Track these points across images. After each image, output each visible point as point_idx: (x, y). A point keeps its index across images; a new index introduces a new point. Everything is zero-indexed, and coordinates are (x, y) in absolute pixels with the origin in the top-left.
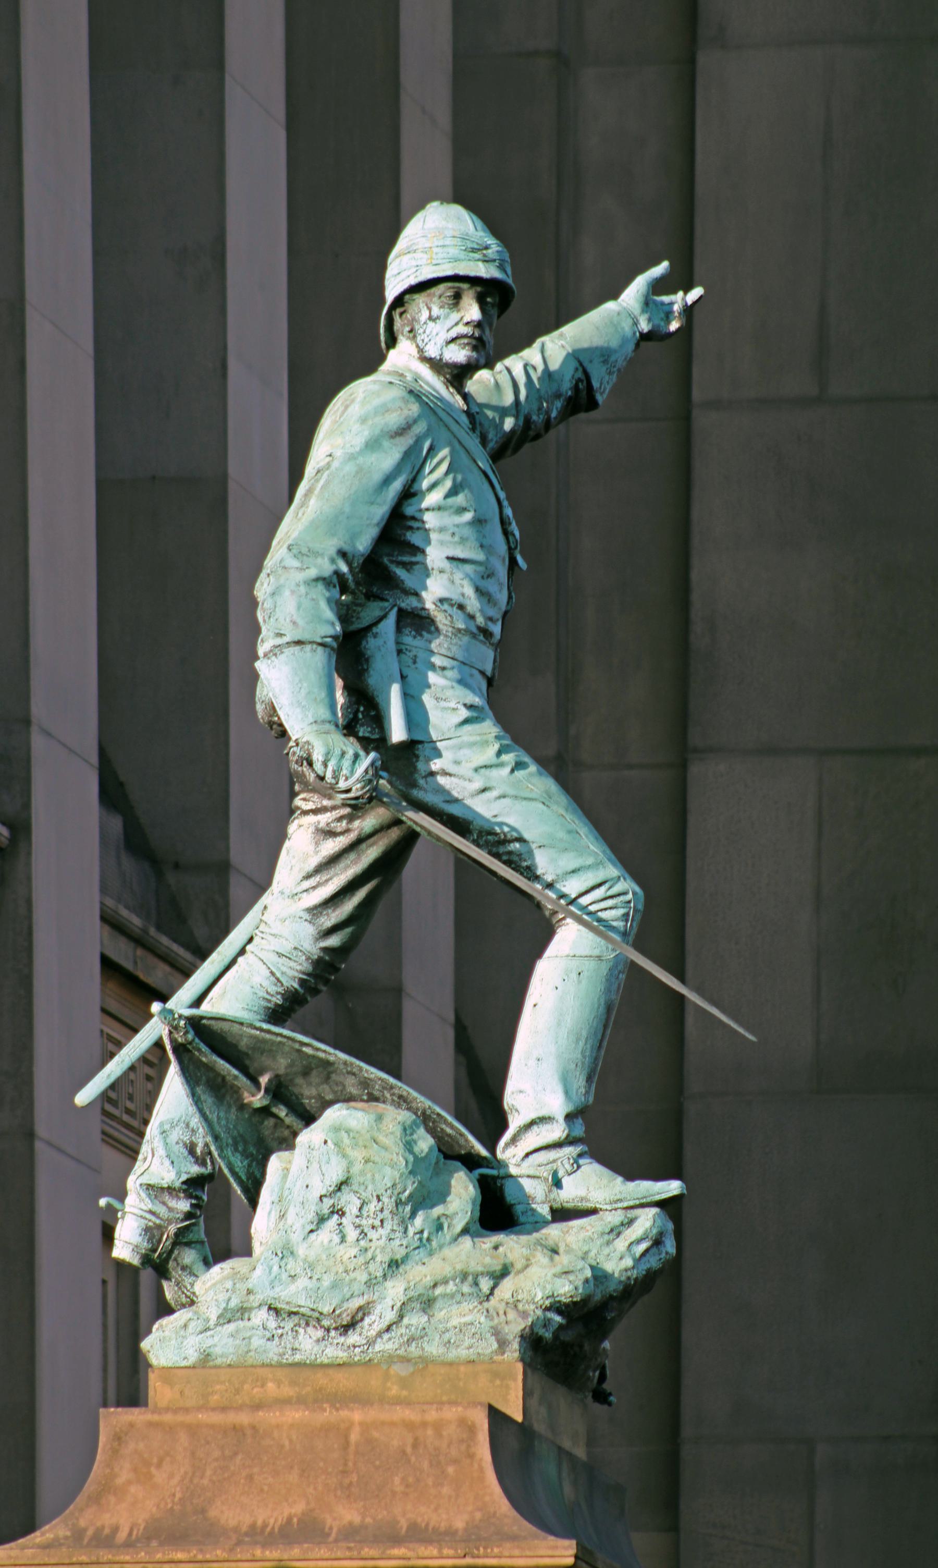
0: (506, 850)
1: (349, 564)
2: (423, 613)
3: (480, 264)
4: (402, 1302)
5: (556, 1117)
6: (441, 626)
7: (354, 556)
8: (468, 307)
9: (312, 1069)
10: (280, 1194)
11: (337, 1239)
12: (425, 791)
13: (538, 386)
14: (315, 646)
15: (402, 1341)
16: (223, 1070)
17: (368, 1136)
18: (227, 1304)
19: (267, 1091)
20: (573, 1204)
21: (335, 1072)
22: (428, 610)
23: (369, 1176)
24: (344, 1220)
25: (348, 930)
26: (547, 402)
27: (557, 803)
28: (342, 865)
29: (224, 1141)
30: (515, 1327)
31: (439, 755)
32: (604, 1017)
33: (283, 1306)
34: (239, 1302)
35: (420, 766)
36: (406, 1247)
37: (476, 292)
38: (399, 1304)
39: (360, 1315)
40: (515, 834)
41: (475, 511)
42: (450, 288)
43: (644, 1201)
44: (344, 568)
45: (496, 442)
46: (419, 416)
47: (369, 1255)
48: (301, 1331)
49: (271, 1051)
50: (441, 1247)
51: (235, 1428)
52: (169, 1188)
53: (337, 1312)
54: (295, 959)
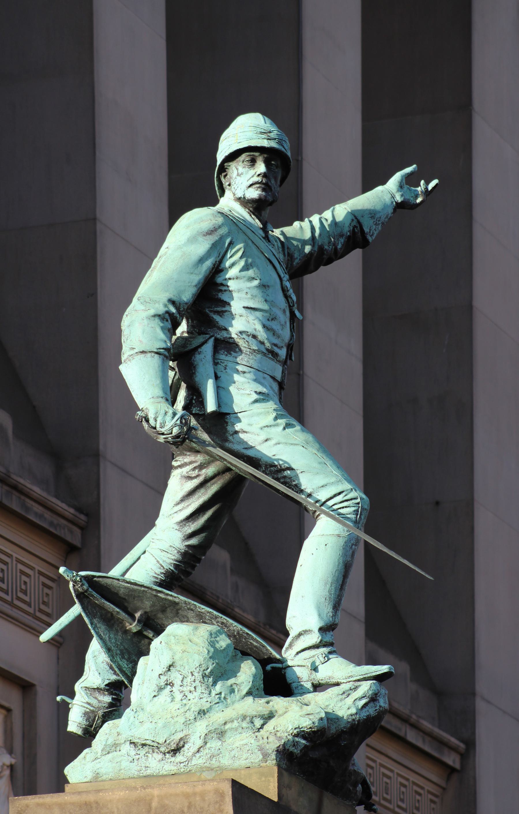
0: (282, 475)
1: (178, 309)
2: (231, 340)
3: (265, 141)
4: (205, 733)
5: (313, 630)
6: (242, 348)
7: (180, 304)
8: (259, 166)
9: (166, 608)
10: (143, 679)
11: (169, 700)
12: (233, 443)
13: (328, 230)
14: (153, 354)
15: (207, 757)
16: (109, 608)
17: (187, 637)
18: (106, 742)
19: (139, 621)
20: (325, 681)
21: (180, 609)
22: (233, 338)
23: (185, 661)
24: (174, 689)
25: (203, 535)
26: (334, 238)
27: (312, 446)
28: (196, 496)
29: (114, 652)
30: (274, 744)
31: (240, 421)
32: (343, 570)
33: (137, 741)
34: (113, 740)
35: (229, 428)
36: (210, 703)
37: (264, 157)
38: (204, 735)
39: (182, 743)
40: (287, 465)
41: (260, 280)
42: (249, 156)
43: (366, 676)
44: (173, 310)
45: (300, 259)
46: (222, 224)
47: (187, 708)
48: (150, 755)
49: (139, 596)
50: (233, 703)
51: (86, 804)
52: (98, 689)
53: (168, 742)
54: (170, 552)
